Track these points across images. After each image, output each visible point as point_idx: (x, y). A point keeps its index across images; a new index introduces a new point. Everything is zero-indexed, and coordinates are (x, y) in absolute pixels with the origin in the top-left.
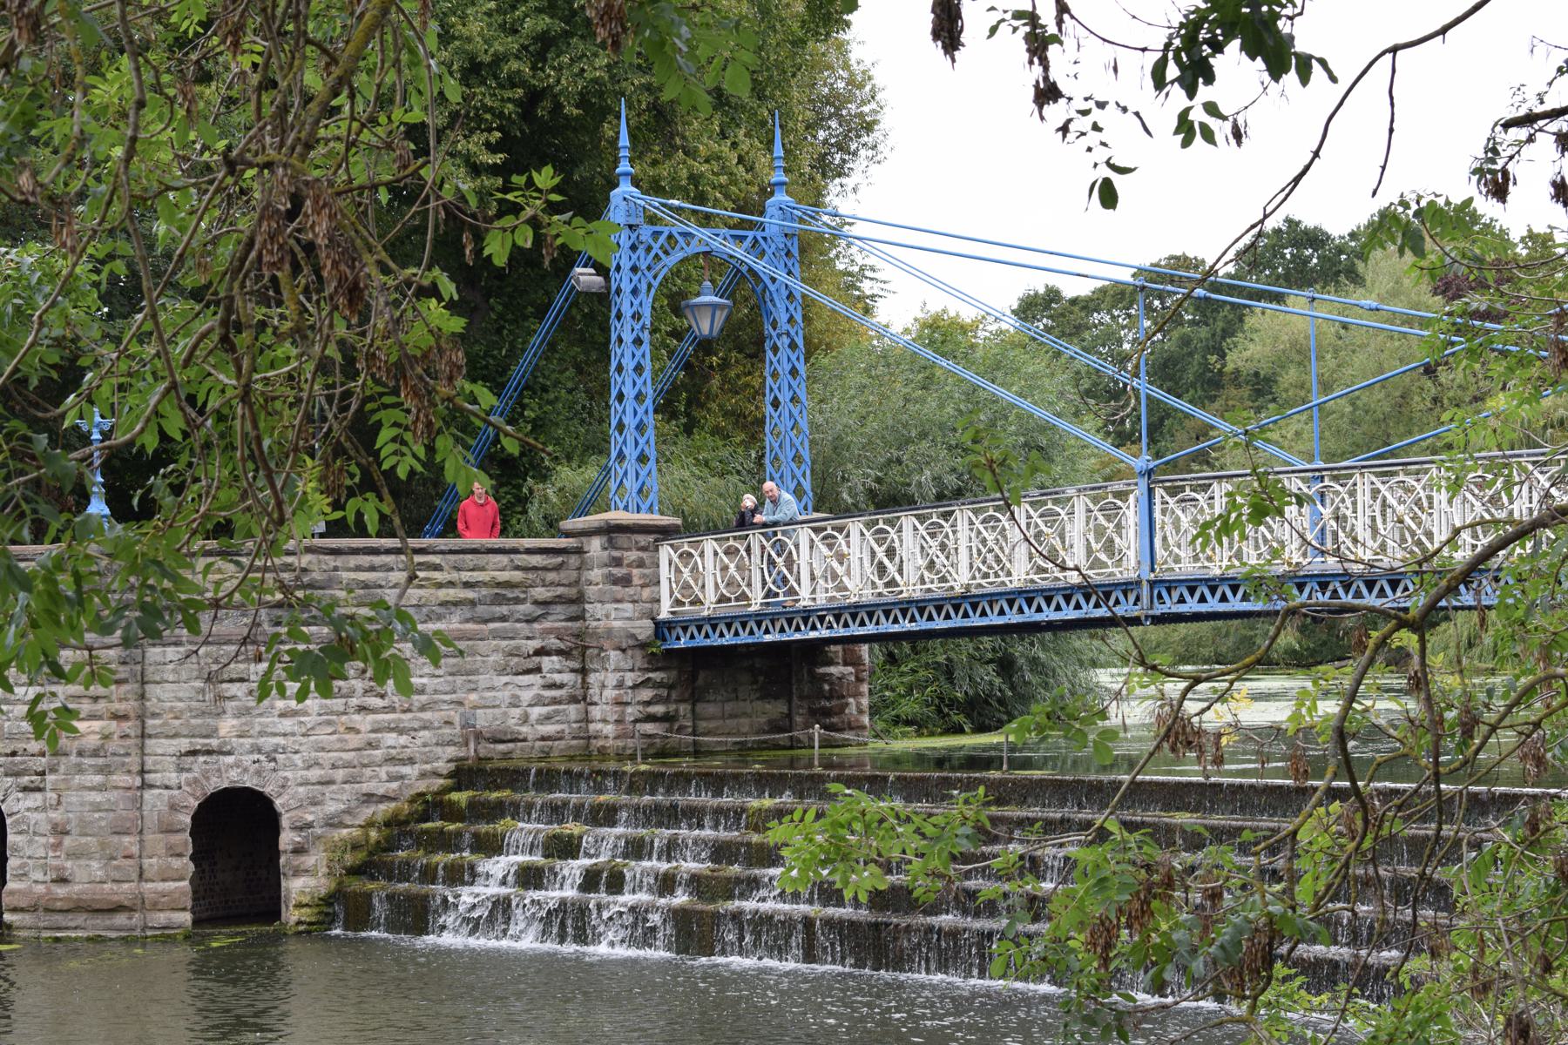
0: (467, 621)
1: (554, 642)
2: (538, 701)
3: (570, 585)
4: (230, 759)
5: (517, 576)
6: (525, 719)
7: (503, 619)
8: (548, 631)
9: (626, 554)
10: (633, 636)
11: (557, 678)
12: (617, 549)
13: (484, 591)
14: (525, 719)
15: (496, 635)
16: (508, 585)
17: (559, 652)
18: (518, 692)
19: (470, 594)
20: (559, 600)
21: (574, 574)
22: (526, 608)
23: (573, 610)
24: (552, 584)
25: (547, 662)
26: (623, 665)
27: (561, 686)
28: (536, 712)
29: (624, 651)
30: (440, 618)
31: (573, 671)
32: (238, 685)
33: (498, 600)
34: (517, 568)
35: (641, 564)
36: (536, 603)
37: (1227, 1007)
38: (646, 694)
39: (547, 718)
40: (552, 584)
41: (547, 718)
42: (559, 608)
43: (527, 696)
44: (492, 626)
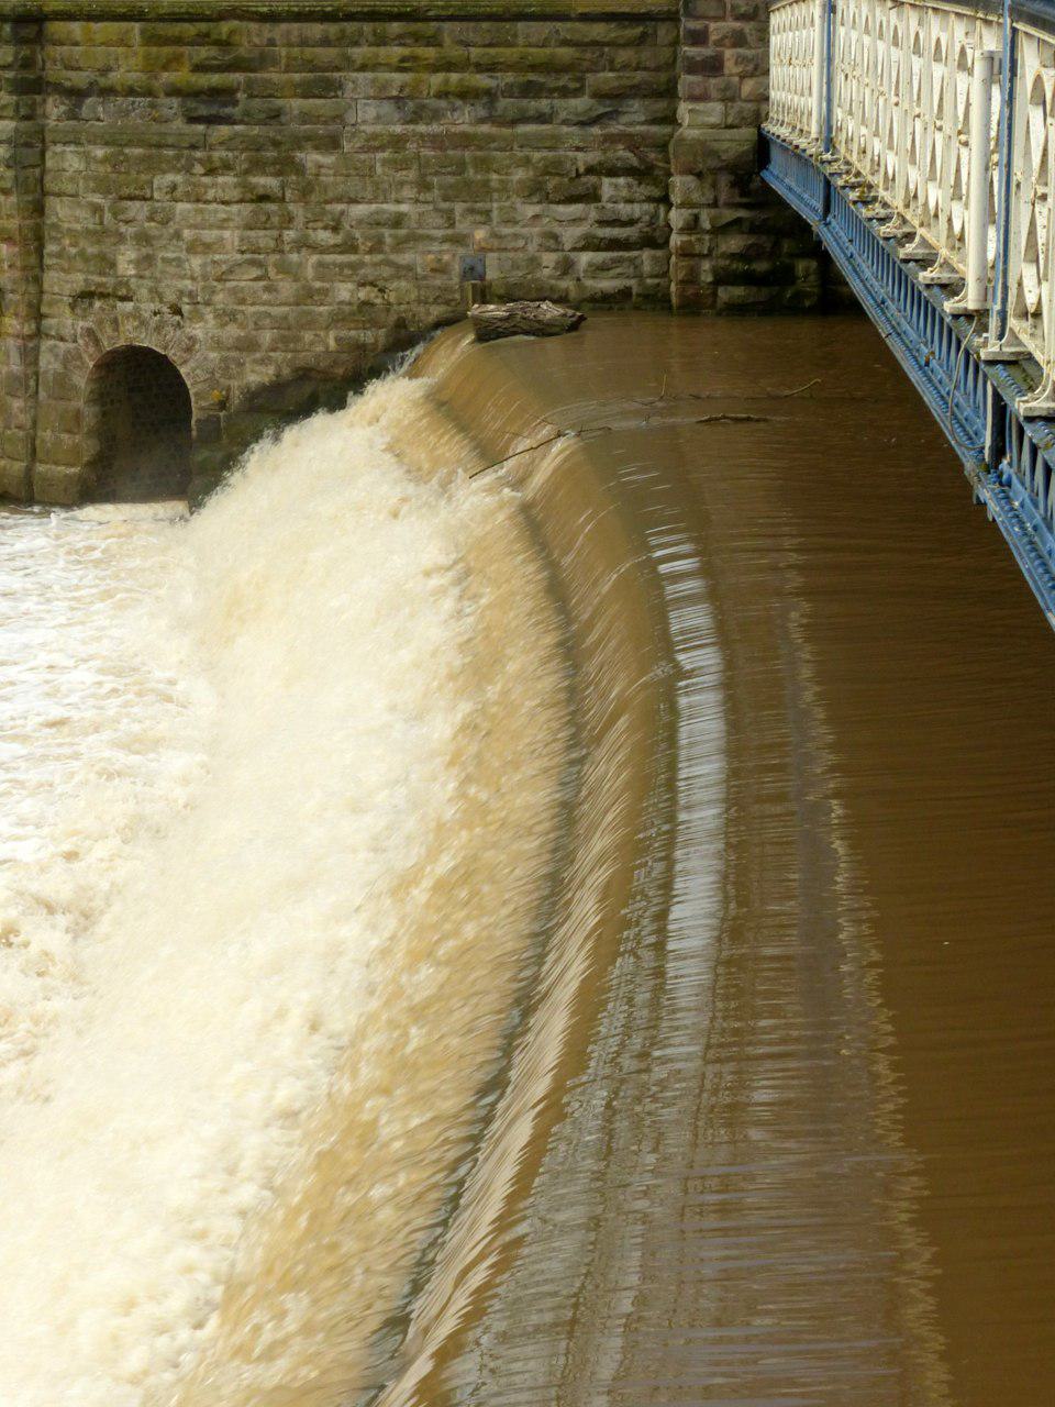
0: (482, 121)
1: (622, 154)
2: (590, 244)
3: (658, 69)
4: (129, 306)
5: (565, 53)
6: (566, 267)
7: (541, 118)
8: (611, 139)
9: (712, 26)
10: (714, 153)
11: (625, 210)
12: (697, 18)
13: (509, 77)
14: (566, 267)
15: (527, 142)
16: (549, 67)
17: (629, 171)
18: (557, 229)
19: (483, 81)
20: (635, 91)
21: (666, 53)
22: (580, 104)
23: (661, 106)
24: (625, 67)
25: (607, 186)
26: (695, 197)
27: (631, 222)
28: (585, 258)
29: (699, 175)
30: (436, 116)
31: (650, 199)
32: (138, 204)
33: (530, 90)
34: (565, 43)
35: (739, 40)
36: (599, 95)
37: (513, 1079)
38: (734, 243)
39: (602, 268)
40: (625, 67)
41: (602, 268)
42: (636, 104)
43: (570, 235)
44: (522, 129)
